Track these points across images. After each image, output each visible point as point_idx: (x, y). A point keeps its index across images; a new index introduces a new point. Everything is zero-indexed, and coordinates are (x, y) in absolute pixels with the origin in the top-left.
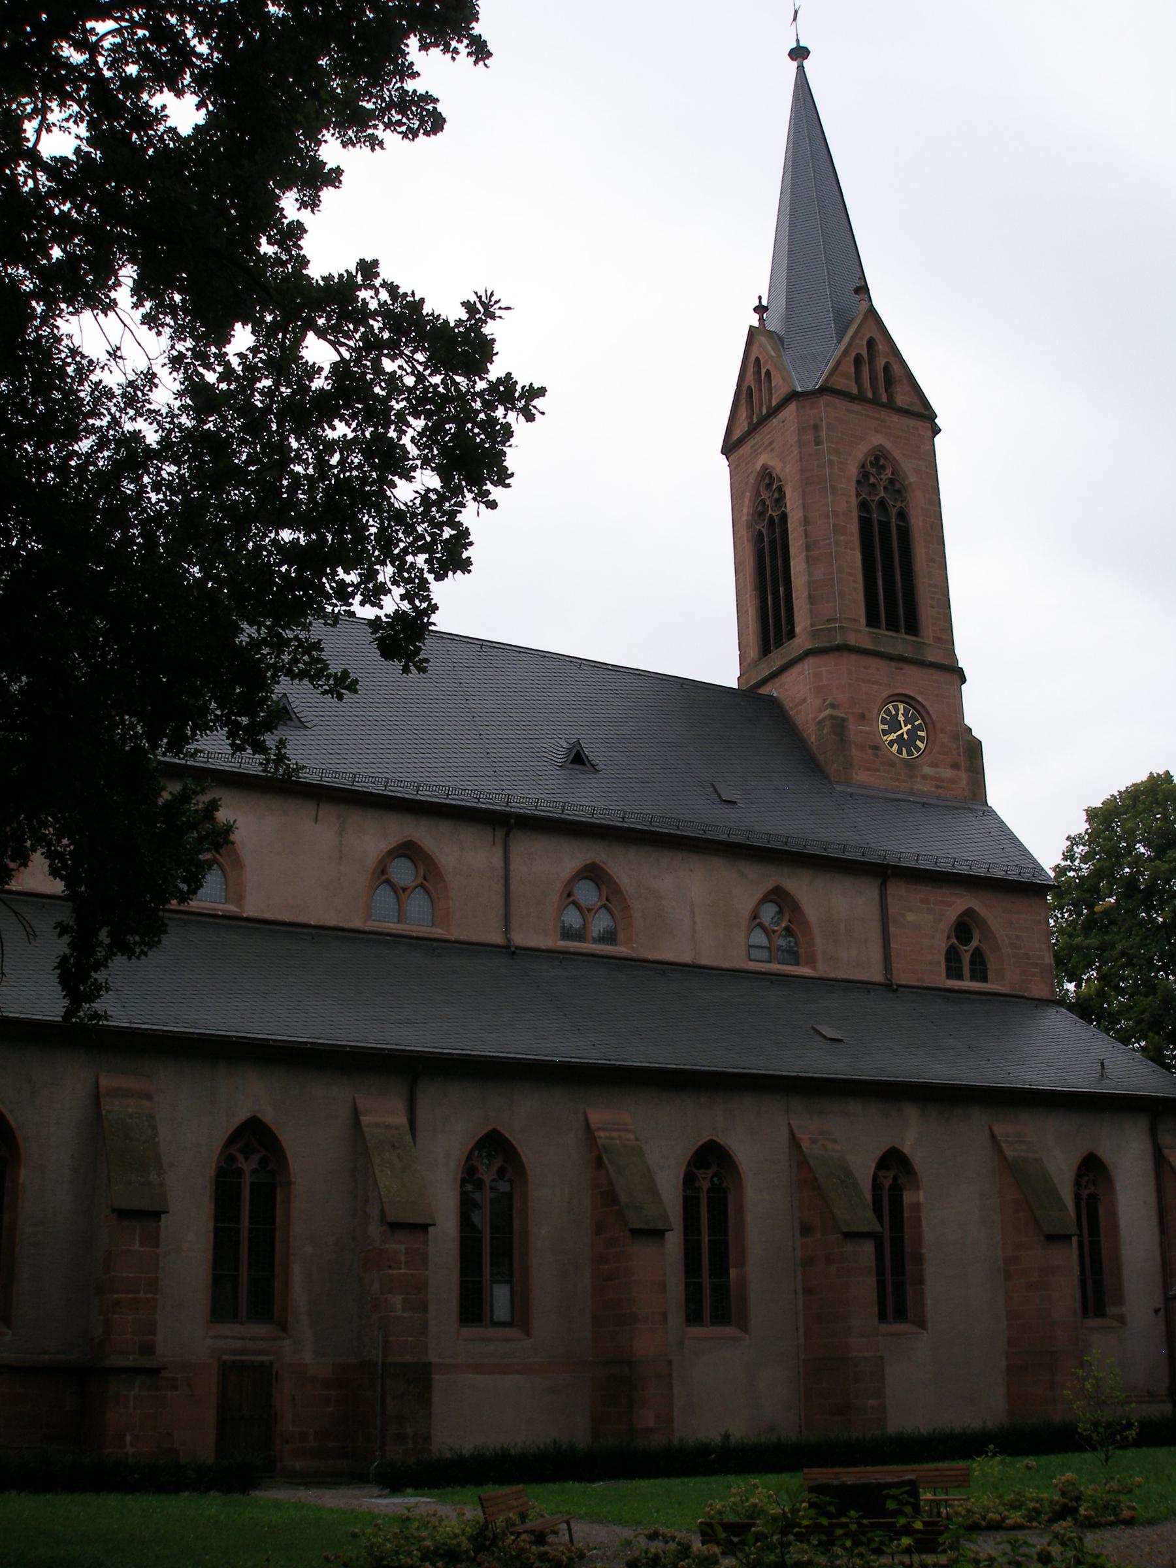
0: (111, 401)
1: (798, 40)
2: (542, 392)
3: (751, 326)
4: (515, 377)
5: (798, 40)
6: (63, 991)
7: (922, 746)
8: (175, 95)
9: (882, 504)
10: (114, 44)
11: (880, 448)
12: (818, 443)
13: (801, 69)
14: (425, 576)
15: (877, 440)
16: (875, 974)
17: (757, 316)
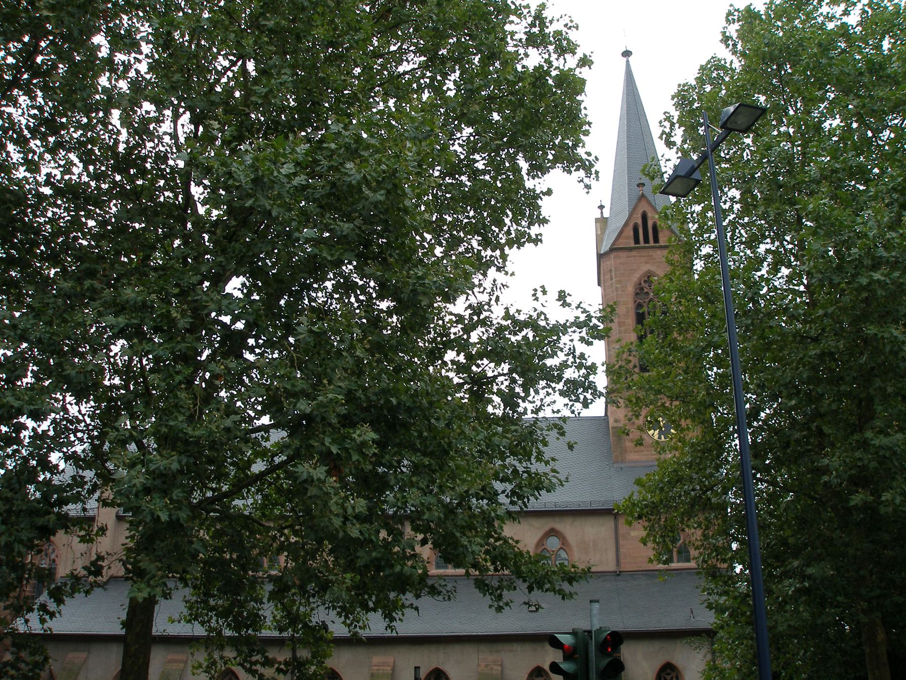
10: (865, 503)
11: (649, 271)
12: (611, 279)
13: (628, 61)
14: (678, 113)
15: (645, 268)
16: (611, 567)
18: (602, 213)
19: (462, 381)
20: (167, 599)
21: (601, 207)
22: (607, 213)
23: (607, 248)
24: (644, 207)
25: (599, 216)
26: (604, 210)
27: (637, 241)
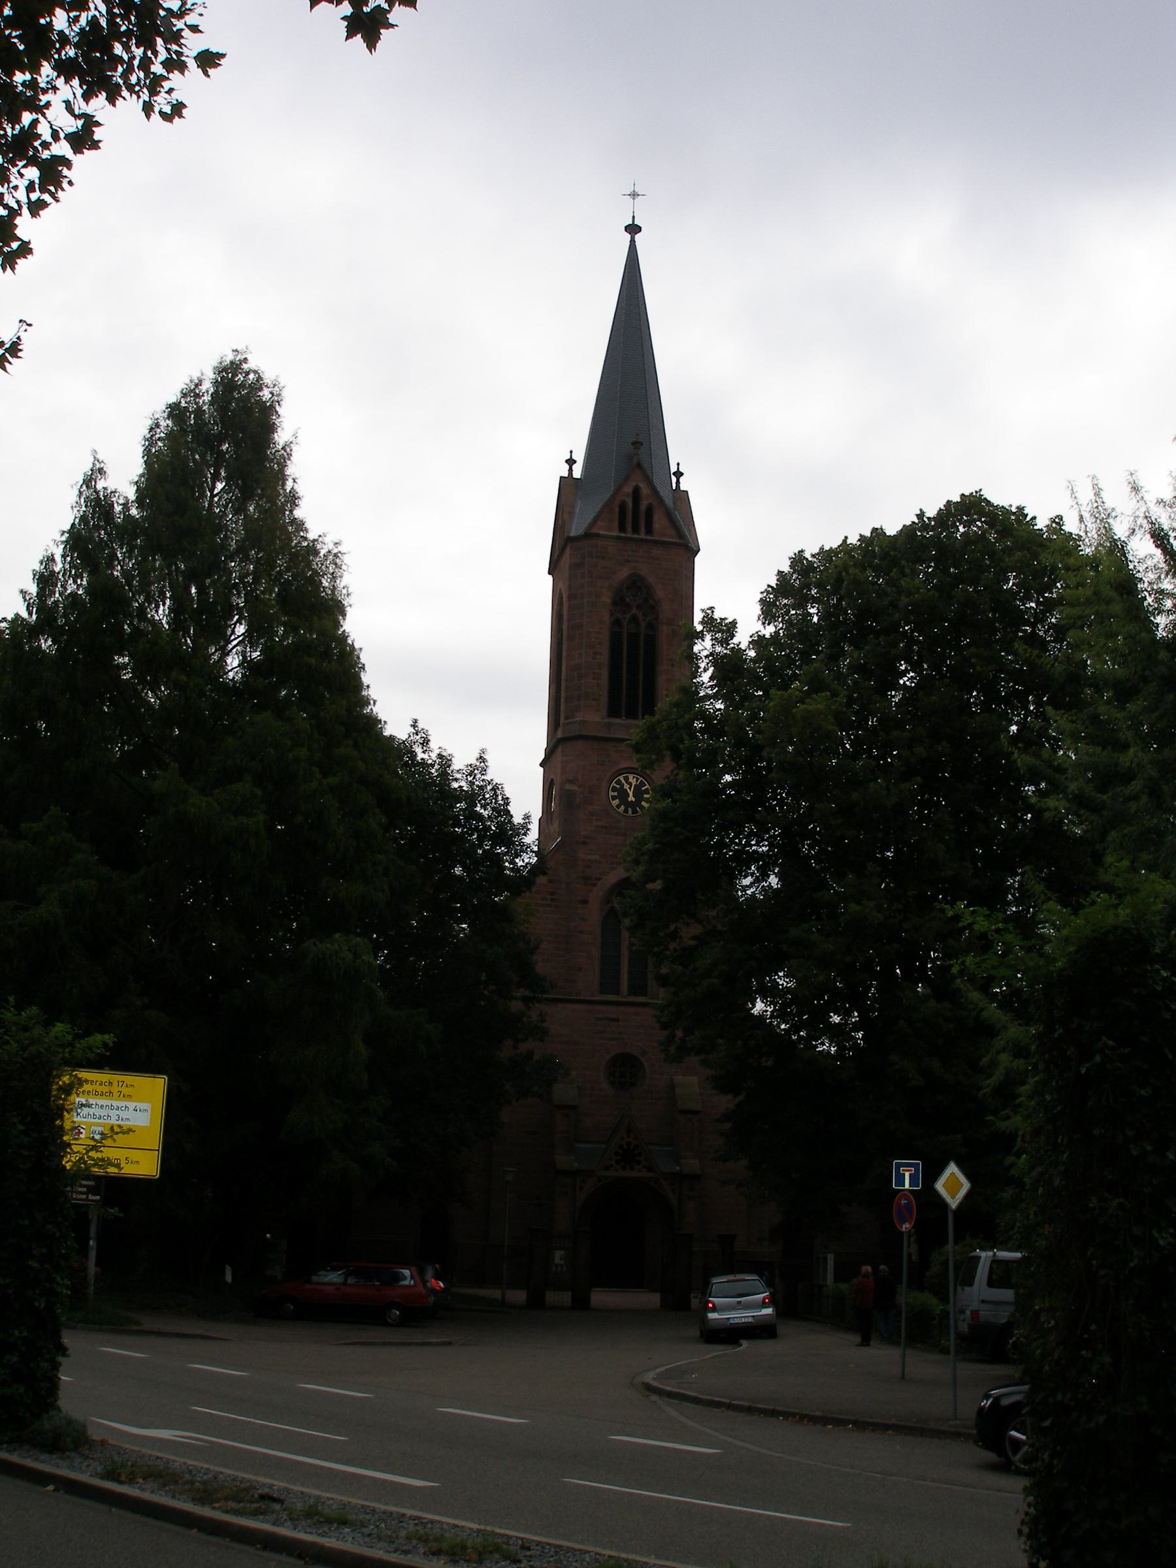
3: (561, 477)
6: (696, 643)
7: (611, 794)
9: (634, 619)
13: (633, 242)
18: (571, 470)
19: (1158, 575)
22: (577, 473)
23: (581, 532)
25: (566, 474)
27: (622, 528)
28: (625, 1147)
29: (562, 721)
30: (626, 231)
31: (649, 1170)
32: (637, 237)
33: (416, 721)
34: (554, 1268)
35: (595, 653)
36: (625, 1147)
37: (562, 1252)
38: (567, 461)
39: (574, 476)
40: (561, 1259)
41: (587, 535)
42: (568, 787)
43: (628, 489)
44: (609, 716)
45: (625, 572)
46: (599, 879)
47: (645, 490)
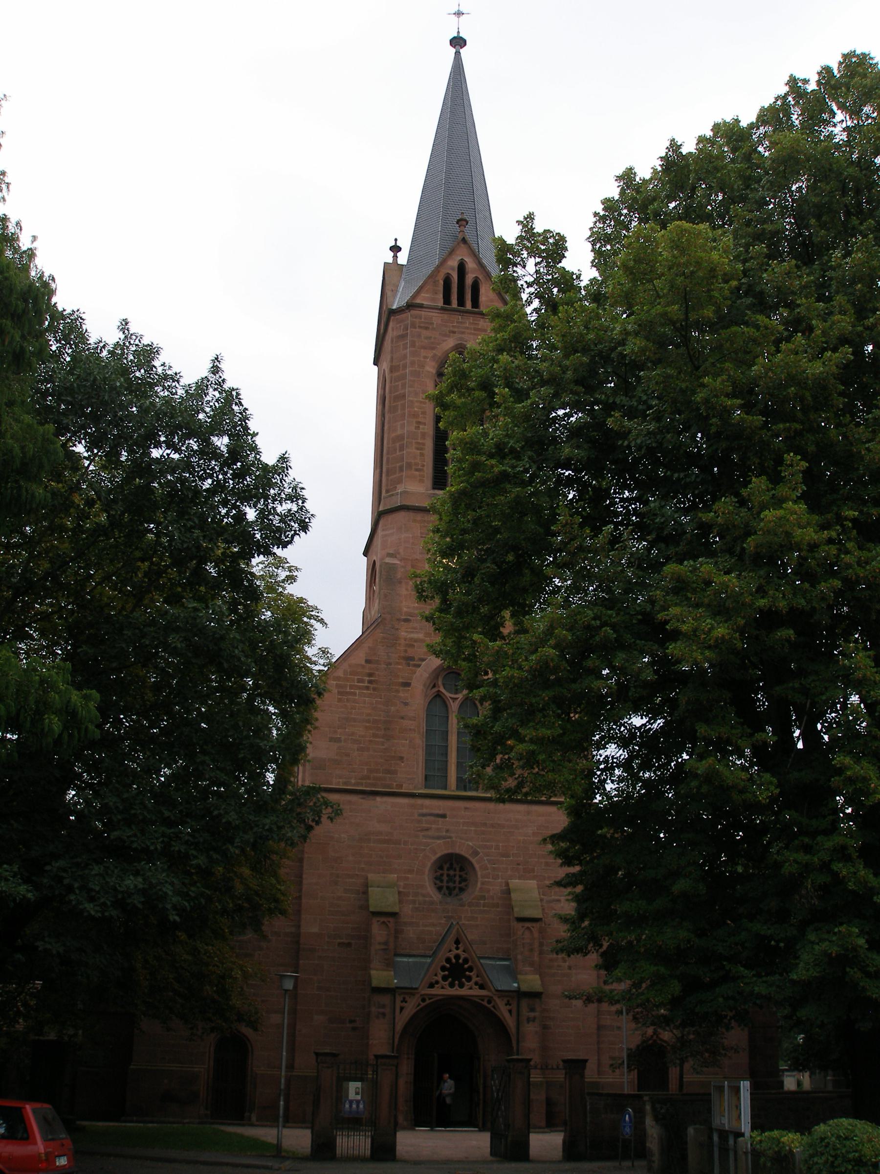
0: (223, 548)
1: (458, 32)
2: (530, 217)
4: (162, 352)
5: (458, 32)
8: (52, 293)
13: (458, 54)
17: (392, 254)
20: (231, 397)
21: (396, 249)
22: (403, 258)
23: (403, 303)
24: (462, 254)
25: (390, 260)
26: (399, 254)
27: (447, 300)
28: (454, 961)
29: (384, 494)
30: (451, 44)
31: (482, 987)
32: (463, 51)
33: (125, 322)
34: (347, 1106)
35: (419, 423)
36: (454, 961)
37: (359, 1084)
38: (392, 249)
39: (399, 262)
40: (357, 1093)
41: (410, 306)
42: (388, 560)
43: (454, 263)
44: (434, 488)
45: (451, 343)
46: (423, 660)
47: (470, 264)
